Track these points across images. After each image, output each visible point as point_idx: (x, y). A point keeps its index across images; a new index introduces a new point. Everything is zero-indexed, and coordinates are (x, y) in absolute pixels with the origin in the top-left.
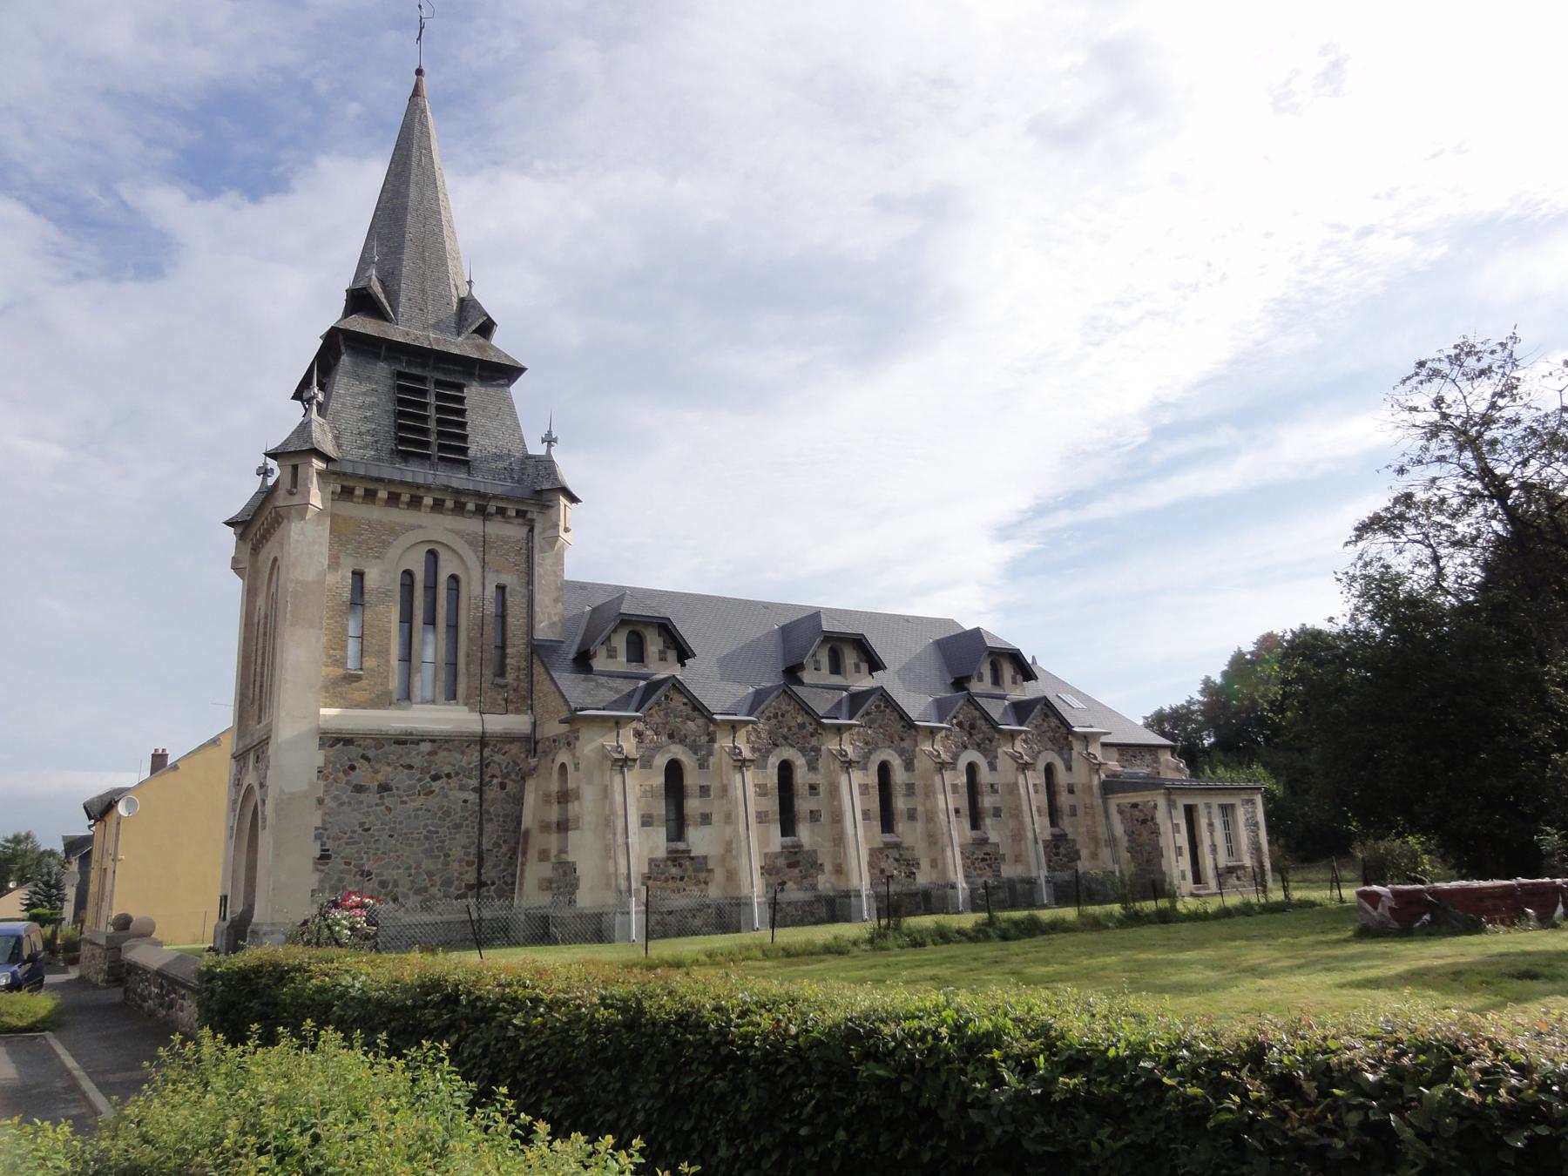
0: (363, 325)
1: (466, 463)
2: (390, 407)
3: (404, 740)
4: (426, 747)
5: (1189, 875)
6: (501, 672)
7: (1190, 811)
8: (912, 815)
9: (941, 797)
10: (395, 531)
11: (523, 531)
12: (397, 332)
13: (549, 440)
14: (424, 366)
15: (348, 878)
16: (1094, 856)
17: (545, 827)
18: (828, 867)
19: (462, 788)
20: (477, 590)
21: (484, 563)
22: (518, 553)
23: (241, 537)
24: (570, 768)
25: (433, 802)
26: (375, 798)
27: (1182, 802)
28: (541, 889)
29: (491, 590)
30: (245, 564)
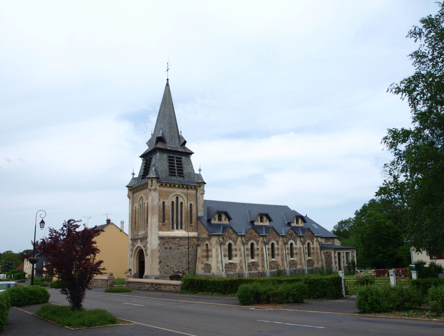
0: (160, 145)
1: (183, 176)
2: (168, 164)
3: (174, 238)
4: (178, 239)
5: (338, 268)
6: (191, 222)
7: (339, 254)
8: (278, 254)
9: (284, 251)
10: (170, 193)
11: (195, 191)
12: (169, 146)
13: (200, 170)
14: (173, 154)
15: (165, 266)
16: (318, 263)
17: (203, 257)
18: (261, 266)
19: (185, 248)
20: (186, 205)
21: (187, 199)
22: (194, 196)
23: (130, 190)
24: (209, 245)
25: (180, 251)
26: (168, 250)
27: (337, 252)
28: (202, 269)
29: (189, 205)
30: (131, 196)
